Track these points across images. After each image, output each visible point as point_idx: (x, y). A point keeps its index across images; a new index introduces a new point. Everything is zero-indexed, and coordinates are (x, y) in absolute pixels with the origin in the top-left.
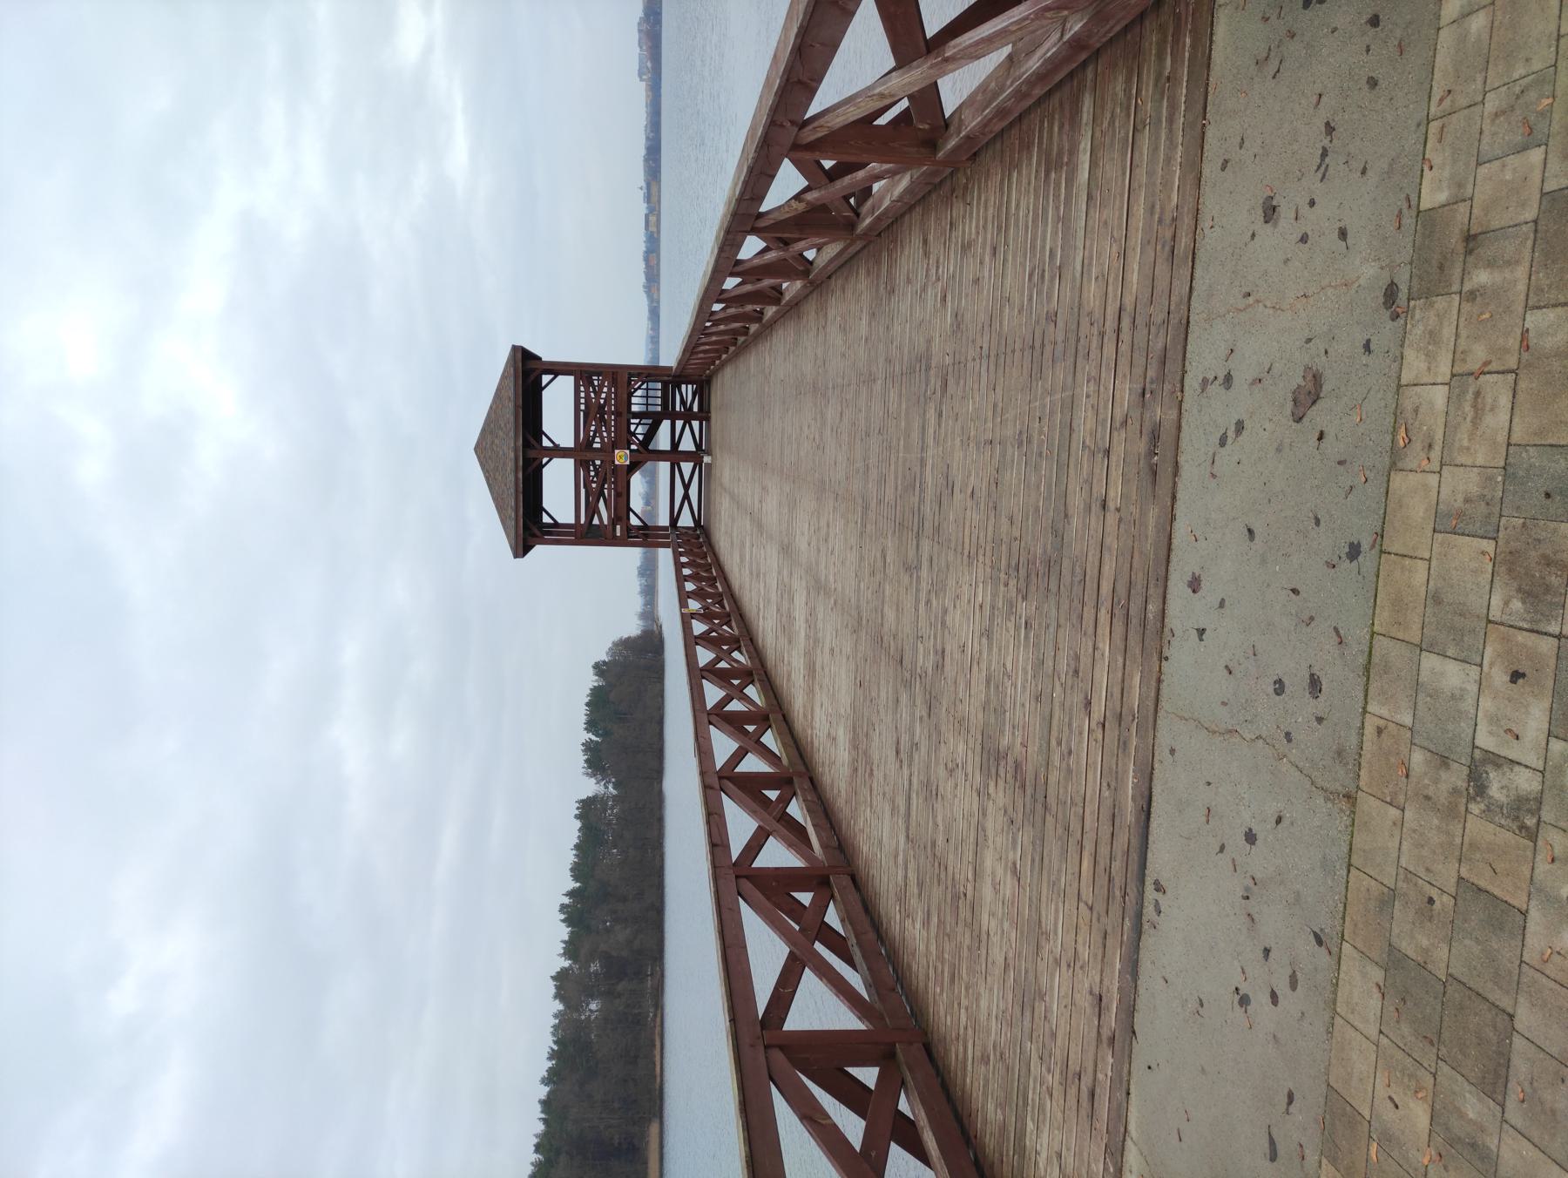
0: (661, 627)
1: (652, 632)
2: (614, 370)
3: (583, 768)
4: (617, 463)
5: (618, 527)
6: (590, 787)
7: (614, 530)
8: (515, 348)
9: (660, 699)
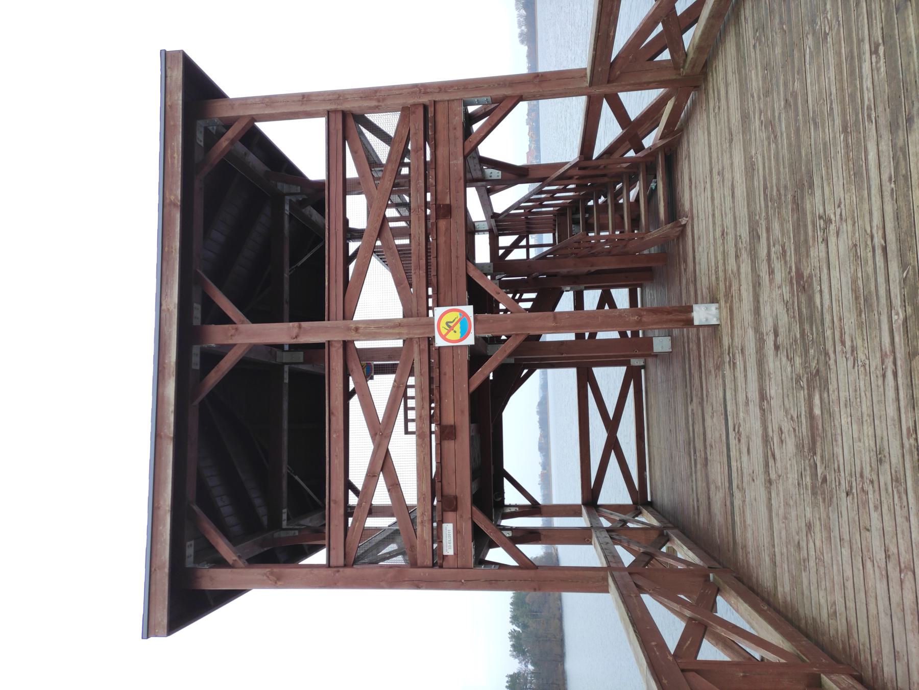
0: (557, 550)
1: (551, 554)
2: (425, 100)
3: (510, 651)
4: (439, 342)
5: (448, 529)
6: (514, 665)
7: (437, 536)
8: (166, 56)
9: (559, 602)
